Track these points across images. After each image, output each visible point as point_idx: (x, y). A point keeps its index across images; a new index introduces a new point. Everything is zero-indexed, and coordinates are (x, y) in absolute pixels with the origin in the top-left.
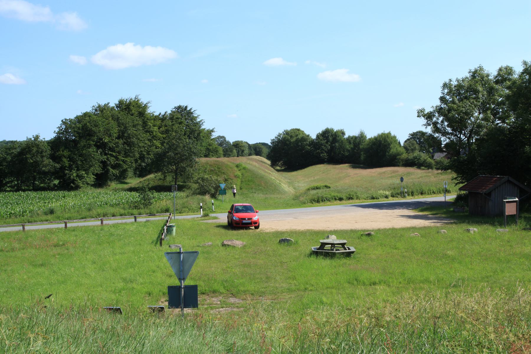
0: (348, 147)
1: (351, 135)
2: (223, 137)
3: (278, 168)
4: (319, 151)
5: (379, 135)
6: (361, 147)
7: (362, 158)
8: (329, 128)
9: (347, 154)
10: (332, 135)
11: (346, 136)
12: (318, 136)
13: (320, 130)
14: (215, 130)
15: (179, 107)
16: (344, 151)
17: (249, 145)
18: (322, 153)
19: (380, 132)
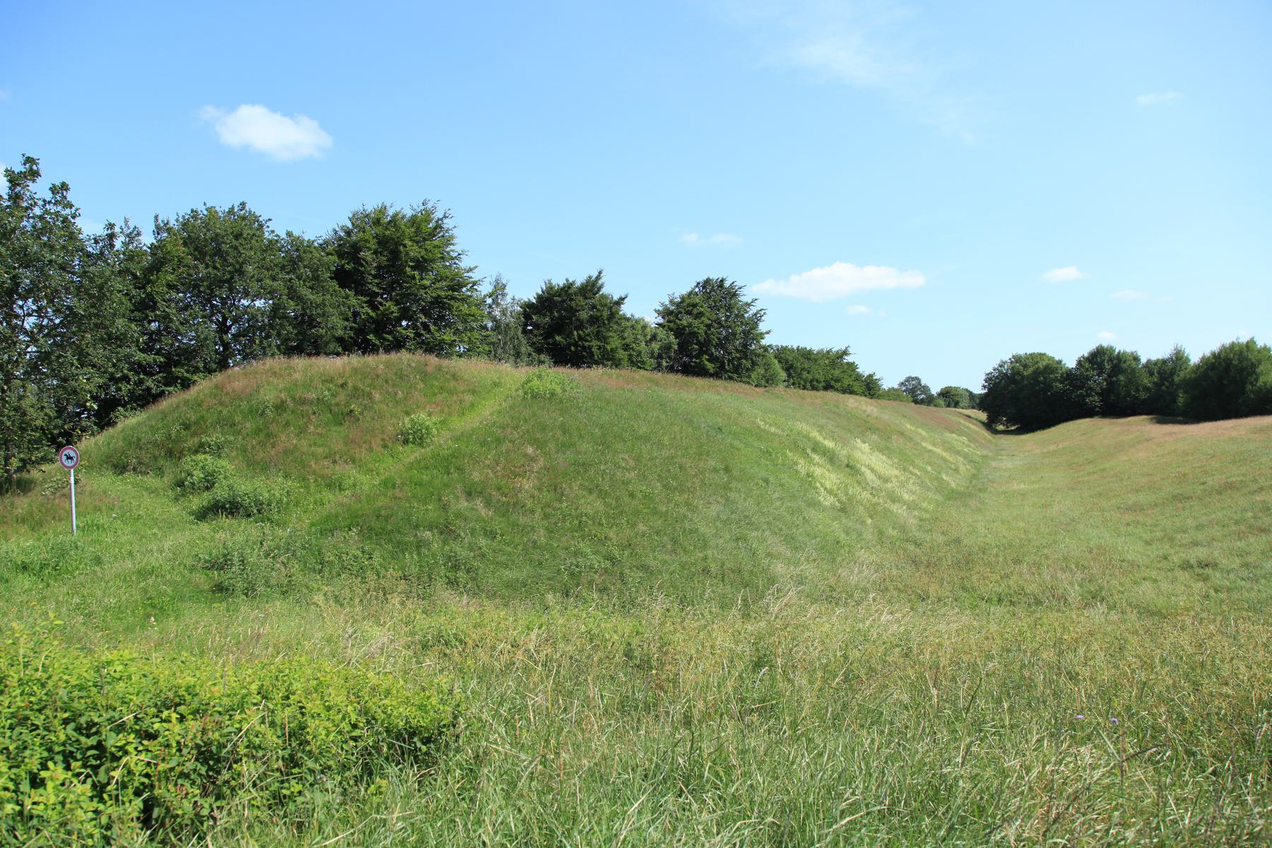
0: (1146, 381)
1: (1154, 358)
2: (917, 378)
3: (1001, 427)
4: (1083, 392)
5: (1223, 349)
6: (1176, 379)
7: (1181, 399)
8: (1105, 345)
9: (1143, 395)
10: (1111, 360)
11: (1143, 360)
12: (1080, 363)
13: (1086, 350)
14: (850, 350)
15: (708, 281)
16: (1137, 390)
17: (971, 393)
18: (1089, 395)
19: (1227, 341)
